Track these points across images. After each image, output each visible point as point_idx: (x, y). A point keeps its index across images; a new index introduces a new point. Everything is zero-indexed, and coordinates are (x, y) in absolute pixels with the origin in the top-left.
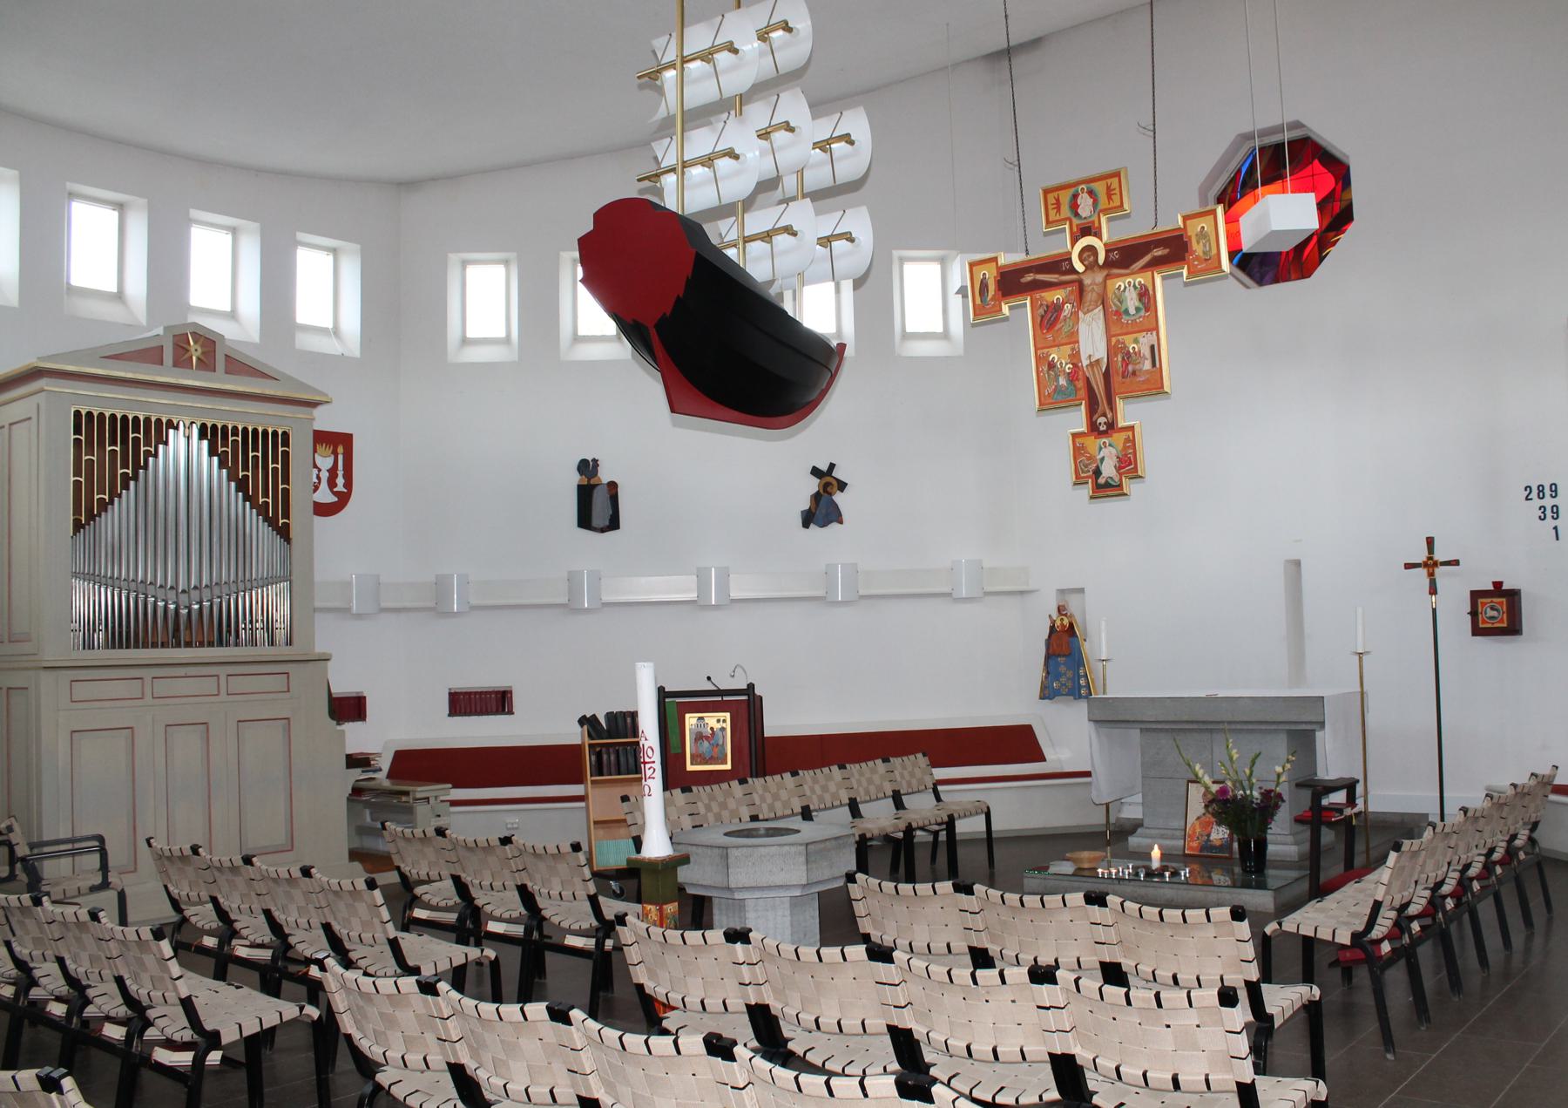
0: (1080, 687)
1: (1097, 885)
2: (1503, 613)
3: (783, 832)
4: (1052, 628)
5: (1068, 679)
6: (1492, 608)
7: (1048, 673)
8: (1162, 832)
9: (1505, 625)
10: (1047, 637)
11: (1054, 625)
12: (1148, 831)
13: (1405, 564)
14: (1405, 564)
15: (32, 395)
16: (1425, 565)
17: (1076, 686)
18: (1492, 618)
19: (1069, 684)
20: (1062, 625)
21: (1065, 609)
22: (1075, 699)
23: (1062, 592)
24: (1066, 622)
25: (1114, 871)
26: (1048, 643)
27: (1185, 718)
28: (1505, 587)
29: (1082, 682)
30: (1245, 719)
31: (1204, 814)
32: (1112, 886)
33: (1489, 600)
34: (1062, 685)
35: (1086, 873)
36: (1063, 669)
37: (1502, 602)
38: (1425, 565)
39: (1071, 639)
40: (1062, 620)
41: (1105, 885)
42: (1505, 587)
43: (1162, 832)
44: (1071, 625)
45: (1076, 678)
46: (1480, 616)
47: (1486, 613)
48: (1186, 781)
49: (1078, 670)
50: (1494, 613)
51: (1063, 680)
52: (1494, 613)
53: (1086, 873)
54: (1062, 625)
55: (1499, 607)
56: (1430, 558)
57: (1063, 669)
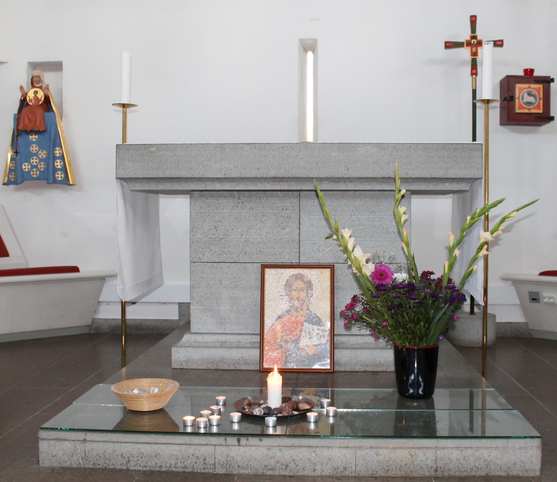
0: (55, 170)
1: (191, 450)
2: (540, 99)
3: (124, 319)
4: (23, 102)
5: (41, 160)
6: (529, 94)
7: (16, 153)
8: (222, 338)
9: (541, 111)
10: (16, 112)
11: (25, 99)
12: (199, 338)
13: (446, 43)
14: (446, 43)
15: (132, 442)
16: (469, 44)
17: (51, 169)
18: (529, 103)
19: (42, 166)
20: (36, 98)
21: (40, 81)
22: (48, 183)
23: (34, 66)
24: (41, 95)
25: (202, 421)
26: (18, 119)
27: (272, 174)
28: (536, 74)
29: (58, 164)
30: (366, 174)
31: (288, 311)
32: (223, 449)
33: (526, 86)
34: (33, 167)
35: (146, 423)
36: (34, 148)
37: (540, 88)
38: (469, 44)
39: (47, 114)
40: (36, 92)
41: (211, 449)
42: (536, 74)
43: (222, 338)
44: (47, 99)
45: (51, 161)
46: (517, 101)
47: (523, 98)
48: (259, 265)
49: (54, 149)
50: (532, 99)
51: (34, 161)
52: (532, 99)
53: (146, 423)
54: (36, 98)
55: (535, 93)
56: (474, 37)
57: (34, 148)
